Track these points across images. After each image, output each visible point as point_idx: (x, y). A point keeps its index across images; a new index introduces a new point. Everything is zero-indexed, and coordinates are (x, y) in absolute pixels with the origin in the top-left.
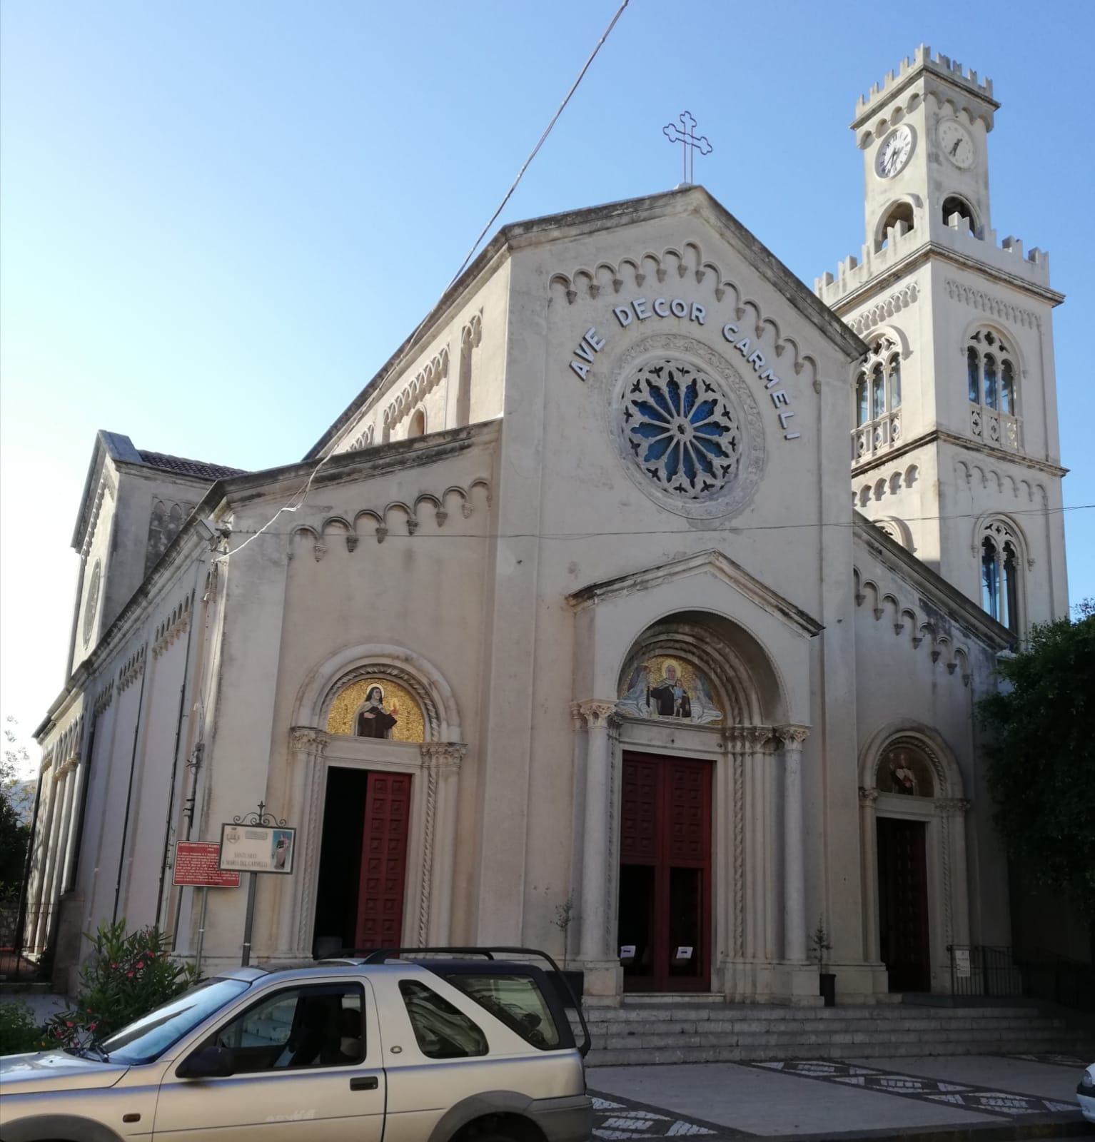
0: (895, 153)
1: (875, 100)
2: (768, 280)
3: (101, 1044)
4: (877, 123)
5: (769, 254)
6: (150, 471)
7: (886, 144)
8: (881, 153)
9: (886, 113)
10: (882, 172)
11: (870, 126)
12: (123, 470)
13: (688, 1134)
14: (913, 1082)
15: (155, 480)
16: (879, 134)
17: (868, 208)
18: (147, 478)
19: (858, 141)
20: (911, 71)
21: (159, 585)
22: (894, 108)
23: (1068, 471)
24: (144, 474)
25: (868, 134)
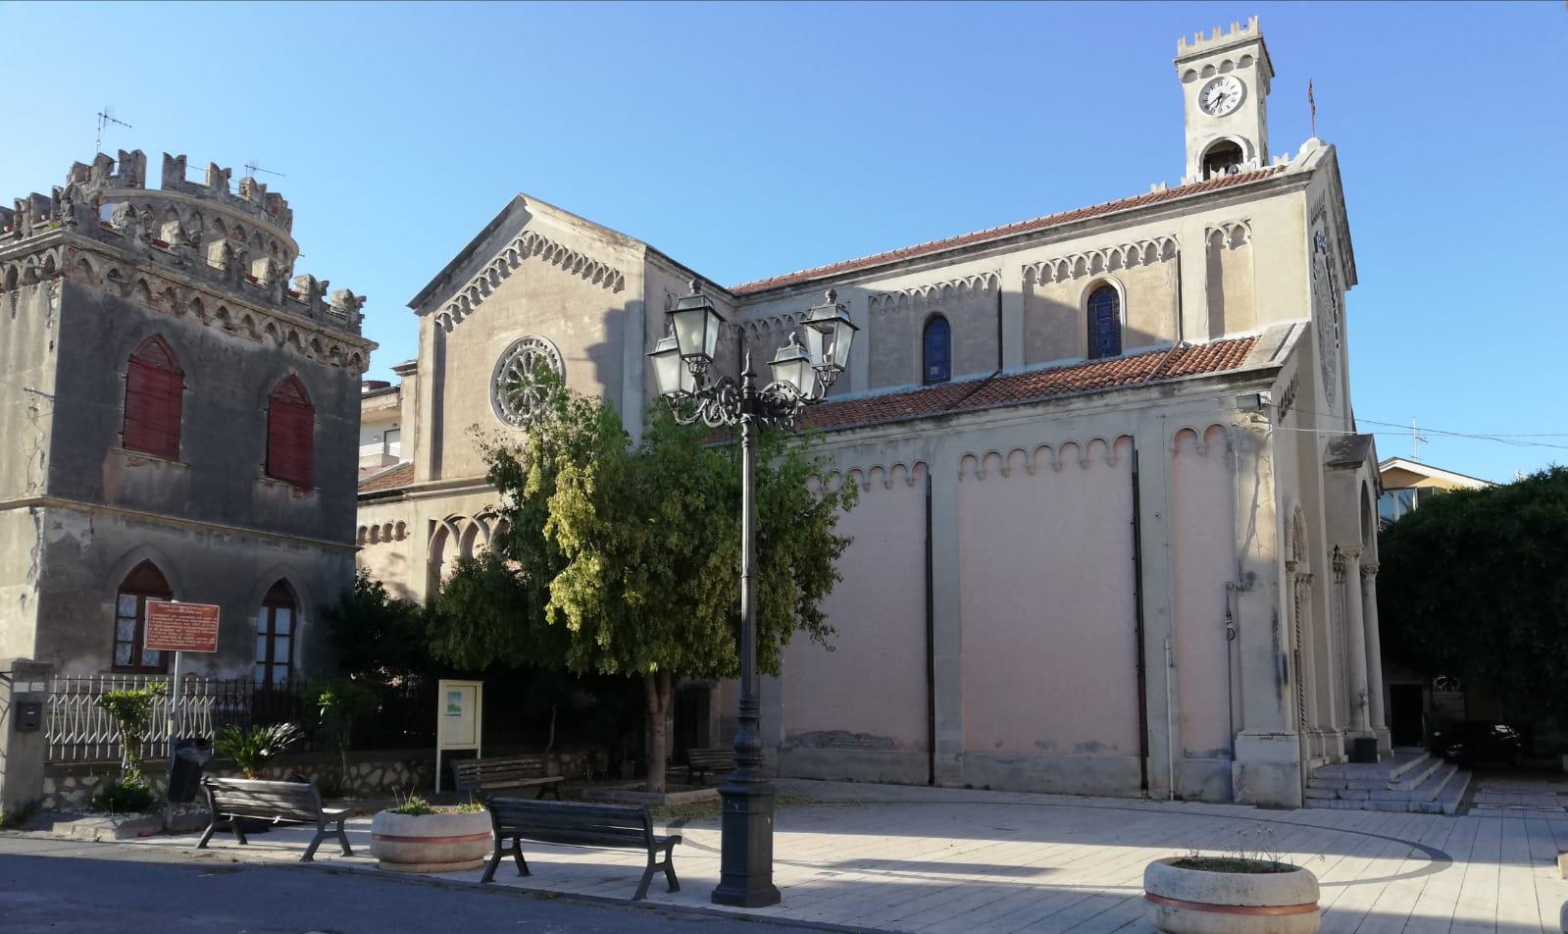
0: (1221, 96)
1: (1201, 46)
2: (1336, 222)
3: (83, 758)
4: (1203, 66)
5: (1343, 205)
6: (668, 263)
7: (1210, 85)
8: (1205, 93)
9: (1216, 61)
10: (1206, 108)
11: (1197, 65)
12: (650, 259)
13: (8, 700)
14: (291, 636)
15: (666, 271)
16: (1204, 76)
17: (1189, 136)
18: (661, 268)
19: (1181, 75)
20: (1243, 35)
21: (998, 417)
22: (1223, 60)
23: (214, 167)
24: (662, 265)
25: (1191, 71)
